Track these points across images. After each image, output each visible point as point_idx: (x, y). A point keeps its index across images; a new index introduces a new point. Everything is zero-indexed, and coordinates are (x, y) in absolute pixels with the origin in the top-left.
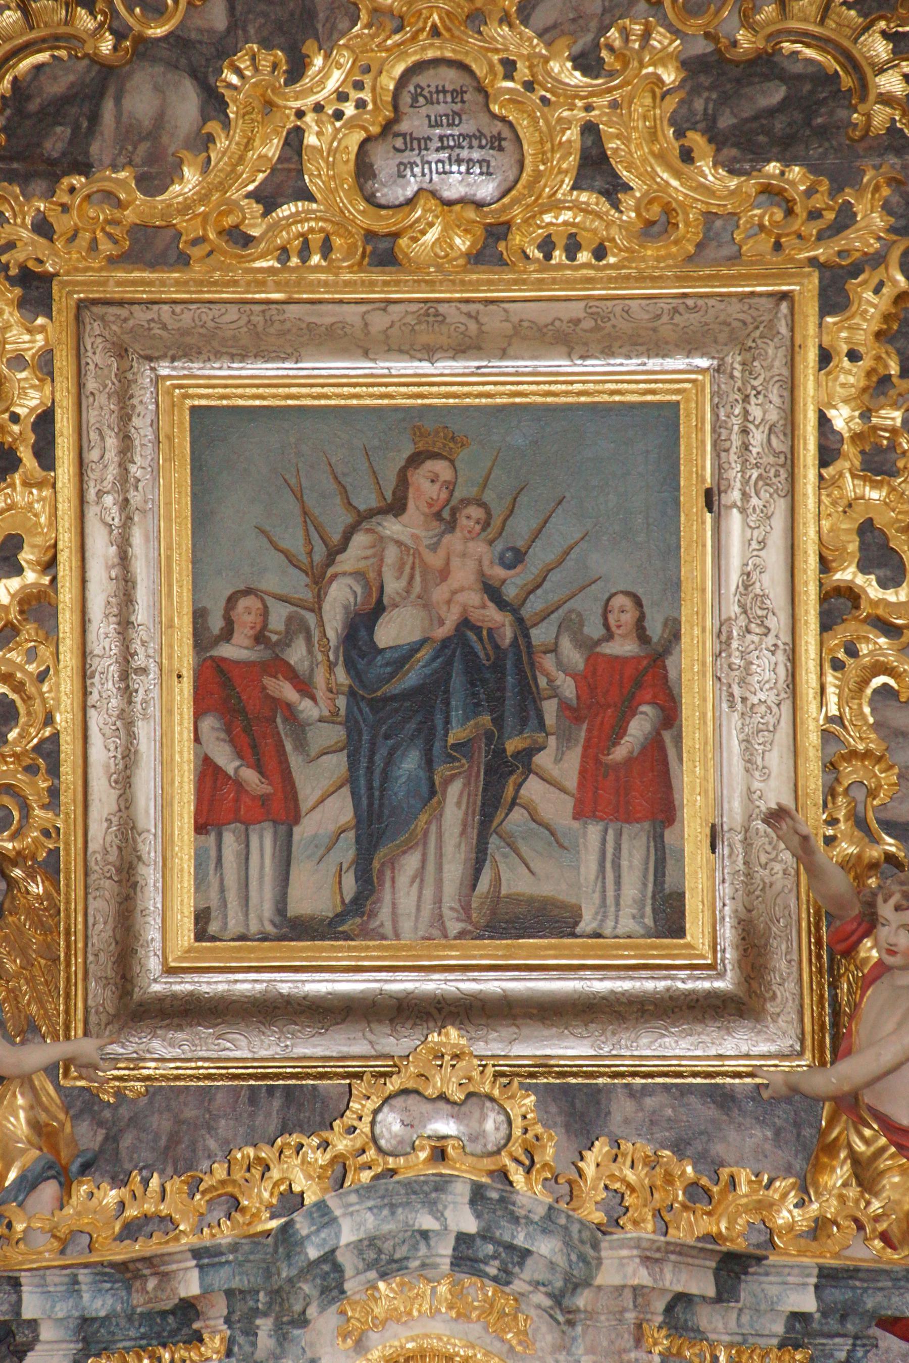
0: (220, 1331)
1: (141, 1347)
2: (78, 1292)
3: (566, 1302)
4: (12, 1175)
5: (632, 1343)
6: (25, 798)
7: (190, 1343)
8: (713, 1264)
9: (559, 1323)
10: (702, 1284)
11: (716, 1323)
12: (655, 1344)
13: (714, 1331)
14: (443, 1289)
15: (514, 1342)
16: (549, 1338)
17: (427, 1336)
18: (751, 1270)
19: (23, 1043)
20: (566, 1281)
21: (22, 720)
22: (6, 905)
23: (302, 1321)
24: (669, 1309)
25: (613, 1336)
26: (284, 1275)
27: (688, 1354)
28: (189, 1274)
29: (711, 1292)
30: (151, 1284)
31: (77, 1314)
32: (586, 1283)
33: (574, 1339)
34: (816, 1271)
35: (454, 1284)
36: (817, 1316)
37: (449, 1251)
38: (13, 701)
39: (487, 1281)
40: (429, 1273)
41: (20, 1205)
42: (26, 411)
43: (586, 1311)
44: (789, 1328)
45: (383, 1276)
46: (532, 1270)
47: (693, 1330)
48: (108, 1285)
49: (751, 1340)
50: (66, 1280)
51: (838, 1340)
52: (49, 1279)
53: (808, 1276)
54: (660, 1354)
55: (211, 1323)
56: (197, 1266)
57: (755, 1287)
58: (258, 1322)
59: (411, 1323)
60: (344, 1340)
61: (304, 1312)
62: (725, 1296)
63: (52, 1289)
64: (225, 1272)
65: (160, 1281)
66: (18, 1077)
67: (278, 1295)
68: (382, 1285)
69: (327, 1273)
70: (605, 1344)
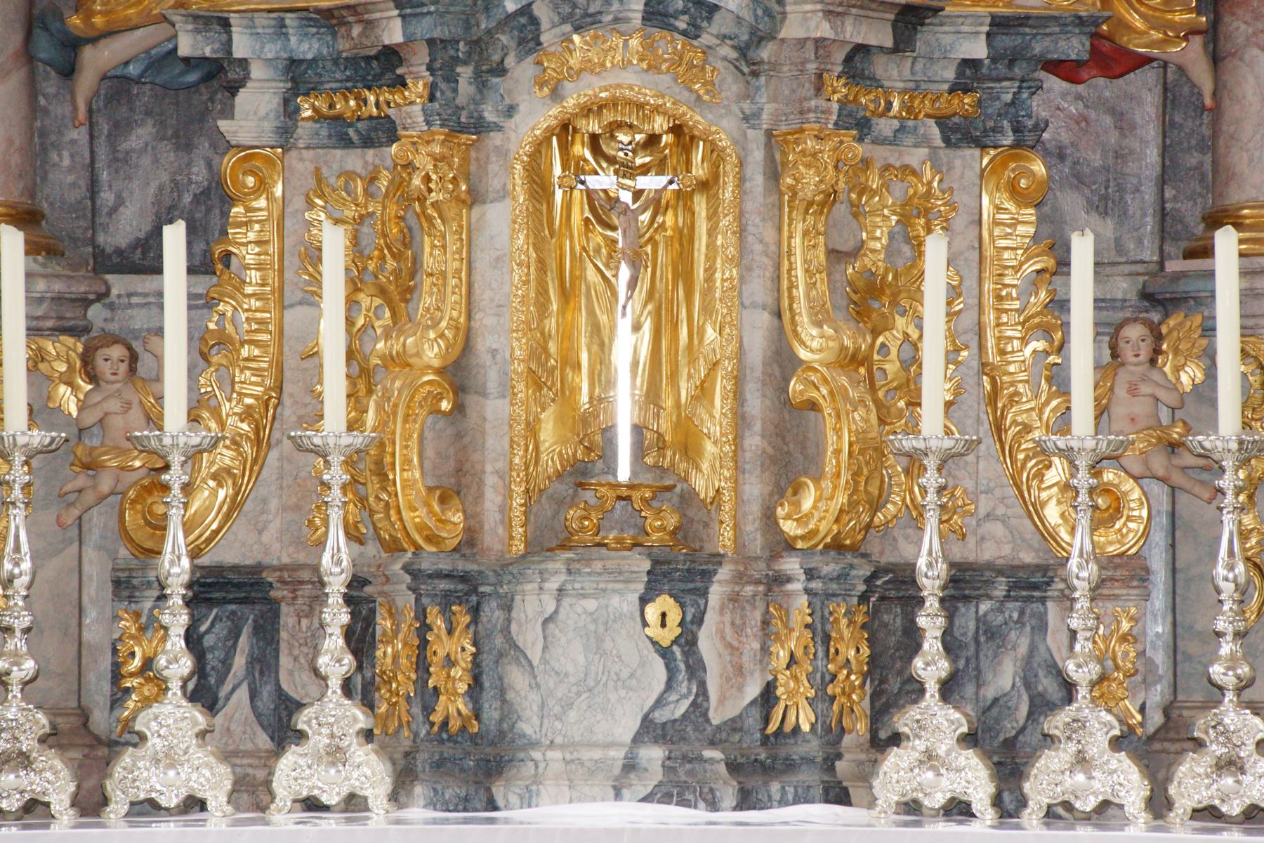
0: (422, 77)
1: (347, 89)
2: (286, 35)
3: (751, 54)
5: (812, 91)
7: (394, 87)
8: (892, 17)
9: (744, 74)
10: (879, 34)
11: (893, 72)
12: (834, 92)
13: (889, 79)
14: (634, 42)
15: (702, 92)
16: (734, 88)
17: (619, 86)
18: (927, 21)
20: (752, 34)
23: (500, 70)
24: (848, 60)
25: (795, 86)
26: (483, 26)
27: (864, 101)
28: (392, 23)
29: (889, 43)
30: (356, 30)
31: (285, 56)
32: (771, 37)
33: (758, 89)
34: (988, 20)
35: (645, 37)
36: (987, 62)
37: (641, 7)
39: (676, 35)
40: (622, 27)
43: (769, 63)
44: (960, 74)
45: (578, 29)
46: (720, 24)
47: (870, 79)
48: (314, 30)
49: (923, 86)
50: (273, 23)
51: (1005, 84)
52: (257, 21)
53: (981, 24)
54: (839, 101)
55: (414, 69)
56: (399, 15)
57: (930, 37)
58: (459, 70)
59: (604, 74)
60: (541, 88)
61: (503, 61)
62: (902, 46)
63: (260, 31)
64: (427, 22)
65: (365, 28)
67: (478, 46)
68: (576, 38)
69: (524, 26)
70: (786, 92)
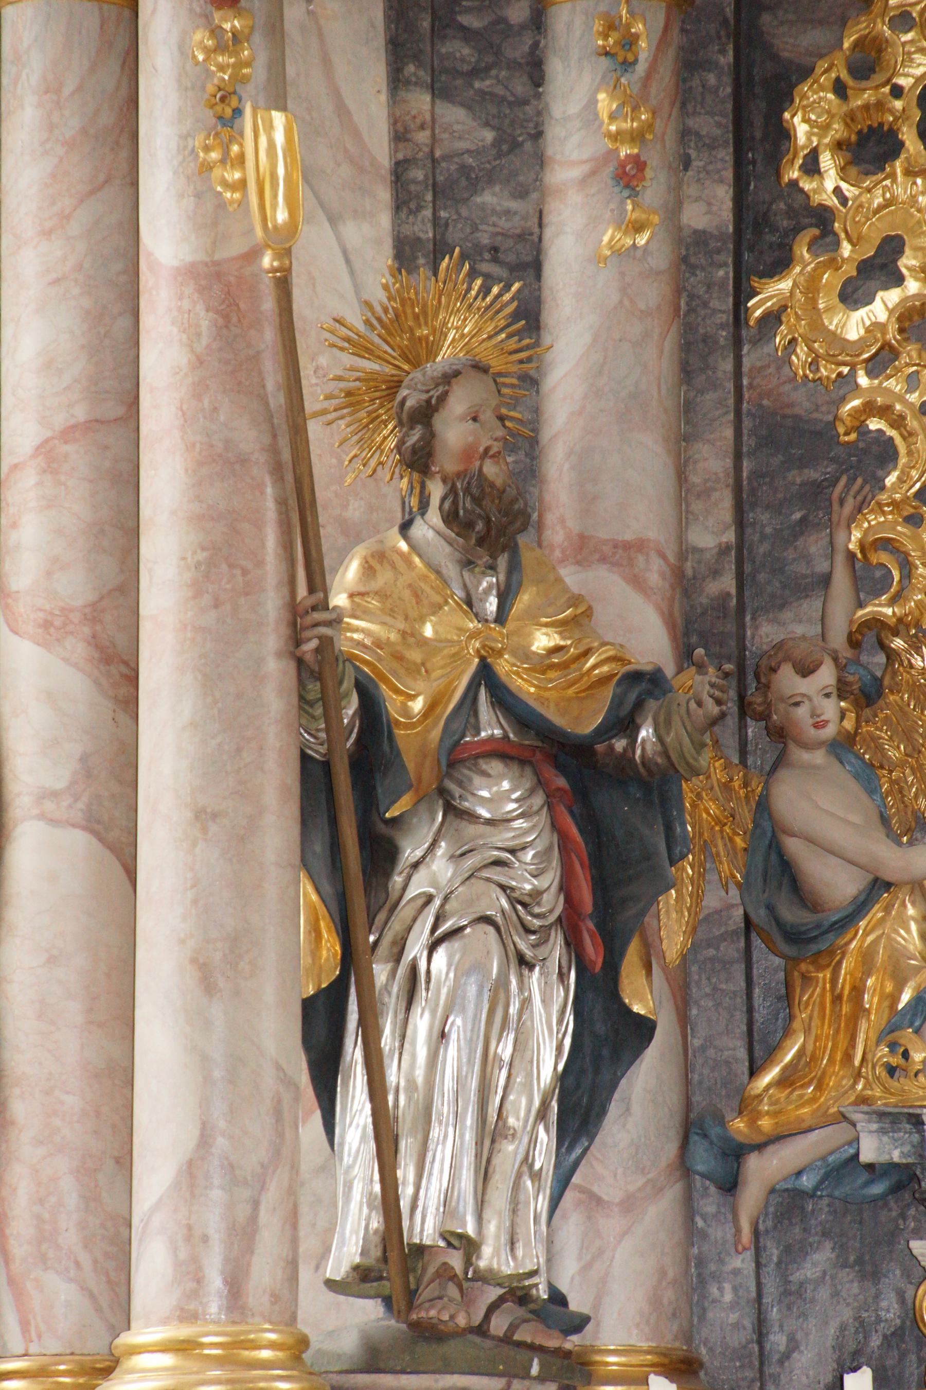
4: (906, 997)
6: (907, 554)
19: (911, 843)
21: (903, 460)
22: (886, 682)
38: (891, 439)
41: (917, 1031)
42: (911, 81)
66: (907, 883)
